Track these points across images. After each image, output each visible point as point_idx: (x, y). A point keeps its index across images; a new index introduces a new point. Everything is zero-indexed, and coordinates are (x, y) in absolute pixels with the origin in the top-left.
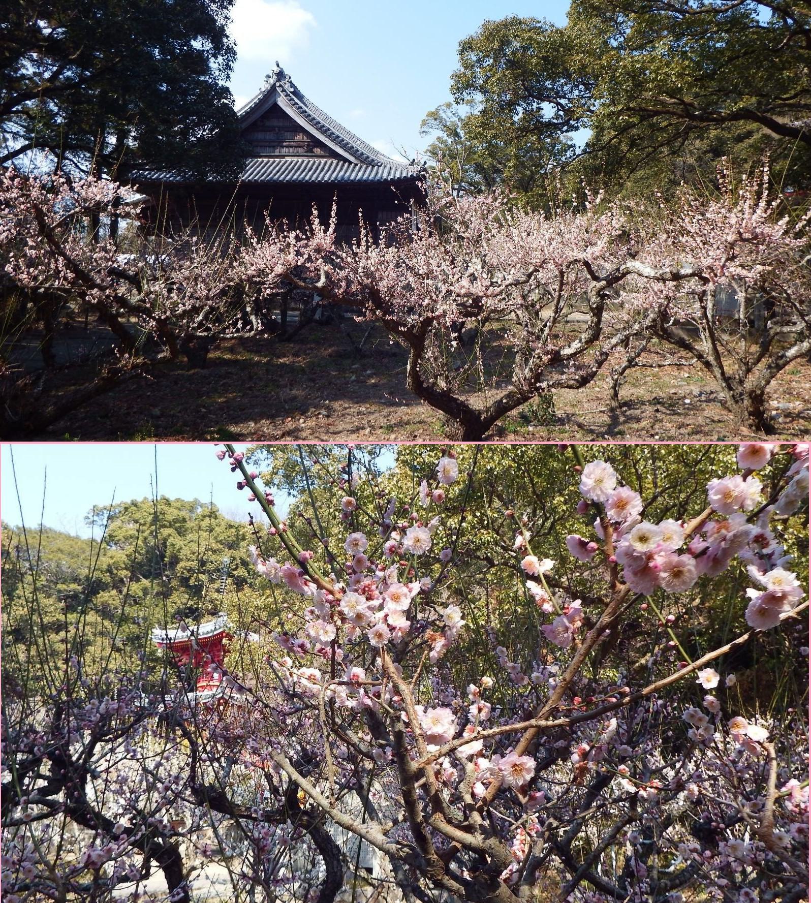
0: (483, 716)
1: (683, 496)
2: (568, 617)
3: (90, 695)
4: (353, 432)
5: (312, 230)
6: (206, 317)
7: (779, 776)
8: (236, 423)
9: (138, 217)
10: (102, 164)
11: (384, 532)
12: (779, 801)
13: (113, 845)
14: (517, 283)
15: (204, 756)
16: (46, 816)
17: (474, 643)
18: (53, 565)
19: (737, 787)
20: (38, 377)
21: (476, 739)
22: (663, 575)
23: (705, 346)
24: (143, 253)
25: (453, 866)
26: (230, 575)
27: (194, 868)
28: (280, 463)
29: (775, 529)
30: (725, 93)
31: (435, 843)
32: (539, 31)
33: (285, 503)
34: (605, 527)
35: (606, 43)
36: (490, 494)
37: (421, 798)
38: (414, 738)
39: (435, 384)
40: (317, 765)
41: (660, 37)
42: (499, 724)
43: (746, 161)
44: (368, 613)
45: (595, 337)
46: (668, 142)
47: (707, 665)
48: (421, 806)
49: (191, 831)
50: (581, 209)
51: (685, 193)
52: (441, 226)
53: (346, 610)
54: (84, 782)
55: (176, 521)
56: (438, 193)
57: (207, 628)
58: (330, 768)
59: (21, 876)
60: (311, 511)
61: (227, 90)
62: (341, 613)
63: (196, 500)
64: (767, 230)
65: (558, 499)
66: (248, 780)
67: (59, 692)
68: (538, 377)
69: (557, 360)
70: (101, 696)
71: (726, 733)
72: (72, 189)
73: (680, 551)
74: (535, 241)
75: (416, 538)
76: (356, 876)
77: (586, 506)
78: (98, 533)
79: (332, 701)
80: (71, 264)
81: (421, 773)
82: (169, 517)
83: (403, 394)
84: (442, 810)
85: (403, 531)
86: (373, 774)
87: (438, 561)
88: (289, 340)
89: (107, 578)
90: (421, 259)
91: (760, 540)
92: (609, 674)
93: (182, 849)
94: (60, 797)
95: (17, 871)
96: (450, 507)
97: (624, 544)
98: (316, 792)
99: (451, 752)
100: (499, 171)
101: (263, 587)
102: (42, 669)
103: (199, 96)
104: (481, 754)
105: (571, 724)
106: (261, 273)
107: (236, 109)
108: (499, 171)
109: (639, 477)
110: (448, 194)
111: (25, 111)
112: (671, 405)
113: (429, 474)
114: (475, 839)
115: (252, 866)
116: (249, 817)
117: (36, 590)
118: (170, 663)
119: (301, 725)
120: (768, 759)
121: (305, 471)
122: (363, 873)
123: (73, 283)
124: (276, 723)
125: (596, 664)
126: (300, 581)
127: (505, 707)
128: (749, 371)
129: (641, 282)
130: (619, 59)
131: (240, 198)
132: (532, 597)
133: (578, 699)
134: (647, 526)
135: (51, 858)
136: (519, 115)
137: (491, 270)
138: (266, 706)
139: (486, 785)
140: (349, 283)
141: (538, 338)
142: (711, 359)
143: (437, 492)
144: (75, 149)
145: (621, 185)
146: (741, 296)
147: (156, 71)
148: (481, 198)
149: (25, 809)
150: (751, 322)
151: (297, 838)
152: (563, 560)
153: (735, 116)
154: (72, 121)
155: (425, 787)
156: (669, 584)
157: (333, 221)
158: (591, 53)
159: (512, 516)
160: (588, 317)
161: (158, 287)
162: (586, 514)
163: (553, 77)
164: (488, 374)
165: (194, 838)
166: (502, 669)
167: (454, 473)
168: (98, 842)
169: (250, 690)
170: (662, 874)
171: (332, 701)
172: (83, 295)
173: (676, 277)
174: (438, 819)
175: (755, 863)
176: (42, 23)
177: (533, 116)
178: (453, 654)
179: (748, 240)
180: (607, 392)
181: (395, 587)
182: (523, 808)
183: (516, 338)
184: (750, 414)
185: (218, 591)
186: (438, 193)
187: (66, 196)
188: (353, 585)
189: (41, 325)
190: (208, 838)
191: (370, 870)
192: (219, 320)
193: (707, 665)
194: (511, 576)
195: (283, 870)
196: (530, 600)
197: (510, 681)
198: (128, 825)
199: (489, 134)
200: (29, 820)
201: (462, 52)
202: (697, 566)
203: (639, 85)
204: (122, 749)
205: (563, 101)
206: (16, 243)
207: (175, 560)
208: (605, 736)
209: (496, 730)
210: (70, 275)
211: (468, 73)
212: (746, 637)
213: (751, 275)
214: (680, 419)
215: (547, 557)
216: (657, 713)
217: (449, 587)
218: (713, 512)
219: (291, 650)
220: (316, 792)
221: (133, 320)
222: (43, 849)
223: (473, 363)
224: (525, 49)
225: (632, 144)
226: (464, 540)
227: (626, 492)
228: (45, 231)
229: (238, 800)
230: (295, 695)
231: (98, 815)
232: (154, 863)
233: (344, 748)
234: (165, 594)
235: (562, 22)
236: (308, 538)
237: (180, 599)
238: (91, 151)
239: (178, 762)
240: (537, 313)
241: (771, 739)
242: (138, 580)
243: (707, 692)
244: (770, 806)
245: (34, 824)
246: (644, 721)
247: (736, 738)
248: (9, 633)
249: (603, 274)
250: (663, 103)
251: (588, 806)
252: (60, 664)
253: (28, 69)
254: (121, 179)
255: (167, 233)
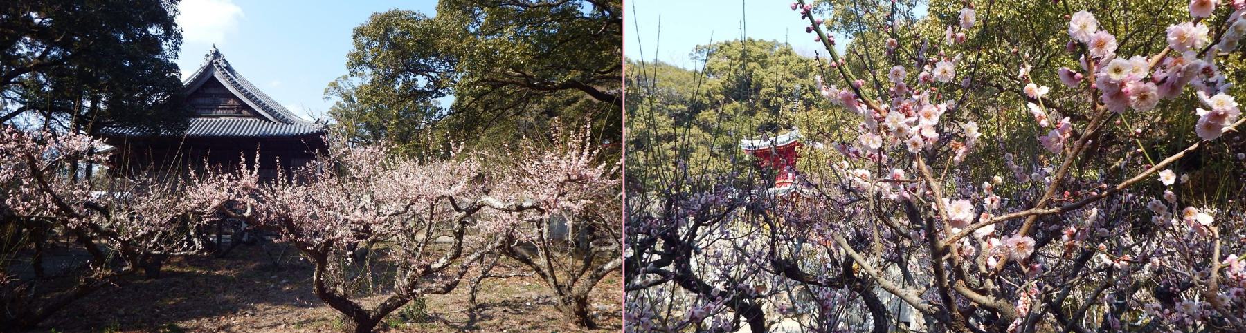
0: (995, 206)
1: (1148, 38)
2: (1061, 132)
3: (693, 190)
4: (272, 327)
5: (241, 173)
6: (159, 240)
7: (1221, 252)
8: (183, 321)
9: (107, 163)
10: (80, 122)
11: (919, 65)
12: (1221, 271)
13: (711, 305)
14: (397, 213)
15: (781, 237)
16: (659, 283)
17: (988, 150)
18: (665, 90)
19: (1189, 260)
20: (31, 285)
21: (989, 223)
22: (1133, 98)
23: (542, 261)
24: (111, 191)
25: (972, 321)
26: (800, 98)
27: (773, 323)
28: (839, 12)
29: (1218, 63)
30: (557, 68)
31: (958, 303)
32: (415, 20)
33: (843, 43)
34: (1088, 61)
35: (466, 30)
36: (1000, 37)
37: (947, 269)
38: (942, 223)
39: (335, 290)
40: (868, 243)
41: (507, 26)
42: (1007, 212)
43: (573, 120)
44: (907, 127)
45: (458, 255)
46: (514, 106)
47: (1166, 167)
48: (947, 274)
49: (771, 294)
50: (447, 157)
51: (526, 144)
52: (339, 170)
53: (890, 125)
54: (689, 256)
55: (759, 57)
56: (337, 145)
57: (783, 138)
58: (878, 246)
59: (641, 328)
60: (863, 49)
61: (175, 66)
62: (886, 127)
63: (775, 41)
64: (589, 173)
65: (1052, 40)
66: (815, 255)
67: (670, 188)
68: (414, 285)
69: (428, 273)
70: (702, 191)
71: (1181, 219)
72: (57, 141)
73: (1146, 80)
74: (411, 182)
75: (944, 70)
76: (897, 328)
77: (1074, 45)
78: (700, 66)
79: (879, 195)
80: (56, 199)
81: (947, 249)
82: (754, 54)
83: (311, 298)
84: (963, 278)
85: (934, 64)
86: (910, 251)
87: (960, 87)
88: (223, 257)
89: (706, 101)
90: (324, 195)
91: (1207, 71)
92: (1092, 174)
93: (764, 308)
94: (671, 268)
95: (638, 324)
96: (970, 46)
97: (1102, 74)
98: (866, 264)
99: (971, 233)
100: (384, 128)
101: (826, 108)
102: (657, 170)
103: (154, 70)
104: (993, 235)
105: (1063, 212)
106: (201, 205)
107: (182, 80)
108: (384, 128)
109: (1114, 24)
110: (345, 146)
111: (21, 82)
112: (515, 306)
113: (954, 20)
114: (989, 300)
115: (818, 321)
116: (815, 283)
117: (652, 109)
118: (755, 165)
119: (855, 213)
120: (1213, 239)
121: (859, 19)
122: (903, 326)
123: (58, 214)
124: (837, 212)
125: (1082, 166)
126: (855, 103)
127: (1011, 199)
128: (575, 280)
129: (493, 213)
130: (476, 42)
131: (185, 148)
132: (1032, 115)
133: (1067, 193)
134: (1120, 61)
135: (664, 314)
136: (399, 85)
137: (378, 204)
138: (829, 198)
139: (997, 259)
140: (269, 213)
141: (414, 255)
142: (546, 271)
143: (959, 35)
144: (59, 111)
145: (478, 139)
146: (569, 224)
147: (121, 52)
148: (370, 149)
149: (643, 277)
150: (577, 243)
151: (852, 299)
152: (1056, 87)
153: (565, 86)
154: (57, 89)
155: (950, 260)
156: (1137, 105)
157: (257, 165)
158: (454, 37)
159: (1017, 53)
160: (452, 239)
161: (123, 216)
162: (1073, 52)
163: (425, 56)
164: (375, 283)
165: (773, 299)
166: (1009, 170)
167: (972, 20)
168: (700, 302)
169: (816, 186)
170: (1132, 327)
171: (879, 195)
172: (65, 222)
173: (520, 209)
174: (960, 284)
175: (1203, 319)
176: (33, 15)
177: (409, 85)
178: (972, 159)
179: (575, 181)
180: (468, 297)
181: (928, 108)
182: (1026, 277)
183: (397, 255)
184: (576, 313)
185: (792, 110)
186: (337, 145)
187: (52, 147)
188: (896, 106)
189: (33, 246)
190: (784, 299)
191: (908, 324)
192: (169, 242)
193: (1166, 167)
194: (1016, 99)
195: (841, 324)
196: (1031, 117)
197: (1016, 180)
198: (723, 289)
199: (376, 99)
200: (646, 286)
201: (355, 37)
202: (1158, 92)
203: (491, 62)
204: (718, 231)
205: (433, 74)
206: (14, 183)
207: (759, 87)
208: (1088, 221)
209: (1004, 216)
210: (55, 207)
211: (360, 52)
212: (1196, 145)
213: (577, 207)
214: (523, 317)
215: (1043, 84)
216: (1128, 204)
217: (969, 108)
218: (1171, 50)
219: (847, 155)
220: (867, 264)
221: (104, 241)
222: (658, 308)
223: (364, 275)
224: (404, 34)
225: (486, 107)
226: (980, 71)
227: (1104, 35)
228: (36, 173)
229: (807, 271)
230: (851, 190)
231: (700, 282)
232: (743, 318)
233: (888, 231)
234: (751, 113)
235: (432, 14)
236: (860, 70)
237: (762, 117)
238: (72, 112)
239: (761, 241)
240: (413, 237)
241: (1215, 224)
242: (730, 102)
243: (1166, 188)
244: (1215, 275)
245: (651, 289)
246: (1118, 210)
247: (1188, 223)
248: (632, 143)
249: (463, 207)
250: (509, 76)
251: (1075, 275)
252: (670, 166)
253: (23, 50)
254: (94, 133)
255: (130, 175)
